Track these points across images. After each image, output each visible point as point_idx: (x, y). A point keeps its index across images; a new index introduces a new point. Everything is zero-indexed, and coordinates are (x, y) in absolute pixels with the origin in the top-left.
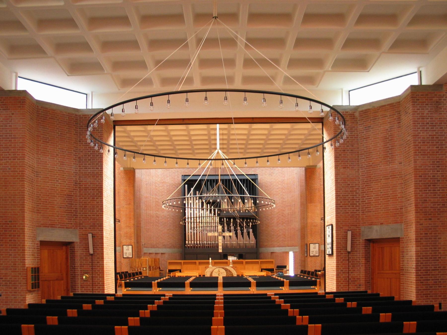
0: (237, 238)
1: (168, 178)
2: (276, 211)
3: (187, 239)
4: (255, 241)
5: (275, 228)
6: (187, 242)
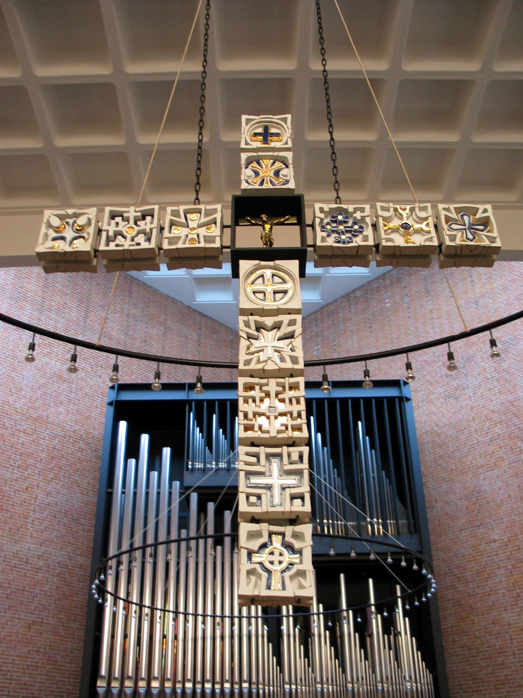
0: (343, 665)
1: (61, 409)
2: (497, 538)
3: (103, 671)
4: (430, 677)
5: (506, 616)
6: (101, 684)
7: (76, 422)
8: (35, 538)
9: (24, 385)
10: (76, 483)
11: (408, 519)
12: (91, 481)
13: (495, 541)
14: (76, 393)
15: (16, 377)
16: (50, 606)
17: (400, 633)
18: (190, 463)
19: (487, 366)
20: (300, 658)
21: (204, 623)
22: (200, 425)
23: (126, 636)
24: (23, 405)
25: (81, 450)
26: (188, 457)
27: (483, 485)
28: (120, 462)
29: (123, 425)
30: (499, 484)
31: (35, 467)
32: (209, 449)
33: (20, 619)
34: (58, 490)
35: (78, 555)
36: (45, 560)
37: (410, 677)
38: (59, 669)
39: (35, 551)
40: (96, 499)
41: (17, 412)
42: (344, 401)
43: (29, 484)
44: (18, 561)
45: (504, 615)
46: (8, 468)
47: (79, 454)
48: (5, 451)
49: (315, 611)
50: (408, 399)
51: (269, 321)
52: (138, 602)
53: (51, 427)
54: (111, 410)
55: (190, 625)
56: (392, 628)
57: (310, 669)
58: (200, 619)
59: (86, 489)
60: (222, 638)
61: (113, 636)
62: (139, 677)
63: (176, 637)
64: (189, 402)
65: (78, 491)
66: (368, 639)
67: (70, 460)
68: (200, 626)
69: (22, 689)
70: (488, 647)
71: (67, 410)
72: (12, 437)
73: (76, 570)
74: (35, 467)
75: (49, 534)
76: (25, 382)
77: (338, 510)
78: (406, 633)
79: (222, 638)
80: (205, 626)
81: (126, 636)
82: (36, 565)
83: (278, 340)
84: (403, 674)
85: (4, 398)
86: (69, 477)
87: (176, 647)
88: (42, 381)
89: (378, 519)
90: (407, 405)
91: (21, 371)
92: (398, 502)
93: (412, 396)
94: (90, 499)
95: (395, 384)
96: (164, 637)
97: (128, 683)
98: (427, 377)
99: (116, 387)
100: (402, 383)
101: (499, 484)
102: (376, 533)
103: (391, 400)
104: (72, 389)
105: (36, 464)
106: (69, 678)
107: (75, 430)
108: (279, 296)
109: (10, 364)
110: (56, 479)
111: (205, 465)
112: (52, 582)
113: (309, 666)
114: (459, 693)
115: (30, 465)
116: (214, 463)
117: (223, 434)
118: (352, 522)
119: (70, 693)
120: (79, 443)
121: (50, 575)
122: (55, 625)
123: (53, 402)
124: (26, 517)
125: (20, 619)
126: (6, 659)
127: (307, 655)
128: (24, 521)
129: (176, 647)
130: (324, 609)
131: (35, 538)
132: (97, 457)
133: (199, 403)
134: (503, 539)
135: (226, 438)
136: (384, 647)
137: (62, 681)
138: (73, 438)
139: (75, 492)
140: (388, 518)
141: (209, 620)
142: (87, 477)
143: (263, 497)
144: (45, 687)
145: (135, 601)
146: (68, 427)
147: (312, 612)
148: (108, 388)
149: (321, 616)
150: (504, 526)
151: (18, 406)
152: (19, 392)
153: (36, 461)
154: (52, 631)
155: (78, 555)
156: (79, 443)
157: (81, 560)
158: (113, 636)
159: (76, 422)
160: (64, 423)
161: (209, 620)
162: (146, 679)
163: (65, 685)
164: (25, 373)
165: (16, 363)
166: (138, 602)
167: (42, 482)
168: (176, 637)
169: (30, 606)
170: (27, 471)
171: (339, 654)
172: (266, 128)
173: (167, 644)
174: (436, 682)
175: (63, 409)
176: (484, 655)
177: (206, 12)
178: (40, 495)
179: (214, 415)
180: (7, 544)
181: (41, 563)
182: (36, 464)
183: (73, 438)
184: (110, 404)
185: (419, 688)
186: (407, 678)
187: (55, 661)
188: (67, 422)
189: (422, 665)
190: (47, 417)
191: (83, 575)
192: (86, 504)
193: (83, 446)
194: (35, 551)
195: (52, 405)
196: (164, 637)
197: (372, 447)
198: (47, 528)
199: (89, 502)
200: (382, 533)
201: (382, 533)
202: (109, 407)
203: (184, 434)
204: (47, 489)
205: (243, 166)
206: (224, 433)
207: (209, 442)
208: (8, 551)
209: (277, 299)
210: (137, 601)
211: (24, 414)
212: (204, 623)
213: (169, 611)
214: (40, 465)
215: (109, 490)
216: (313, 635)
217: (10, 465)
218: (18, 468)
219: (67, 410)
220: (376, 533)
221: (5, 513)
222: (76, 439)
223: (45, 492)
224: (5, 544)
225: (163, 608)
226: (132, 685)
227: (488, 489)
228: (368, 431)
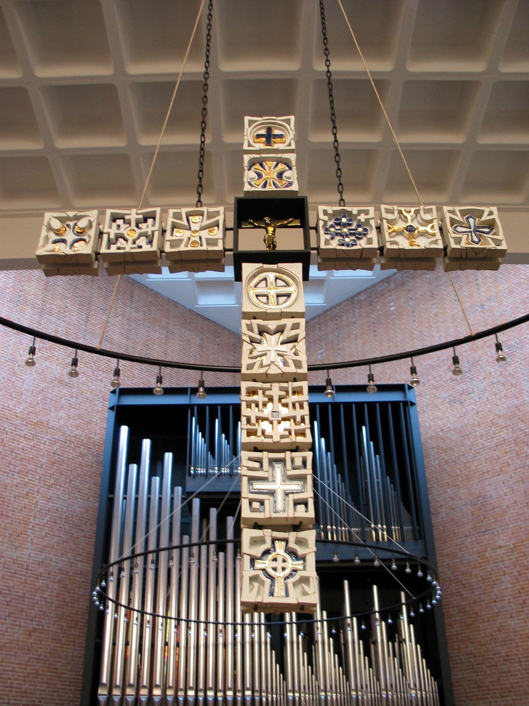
1: (62, 414)
2: (502, 544)
3: (105, 679)
4: (435, 685)
5: (512, 623)
6: (102, 692)
7: (77, 427)
8: (36, 544)
9: (25, 389)
10: (77, 489)
11: (413, 525)
12: (92, 486)
13: (500, 547)
14: (77, 398)
15: (16, 381)
16: (51, 613)
17: (404, 640)
18: (192, 468)
19: (492, 370)
20: (304, 665)
21: (206, 630)
22: (202, 430)
23: (127, 643)
24: (23, 409)
25: (82, 455)
26: (190, 463)
27: (489, 491)
28: (121, 467)
29: (124, 430)
30: (505, 490)
31: (35, 472)
32: (211, 454)
33: (20, 626)
34: (59, 495)
35: (79, 561)
36: (45, 566)
37: (415, 685)
38: (60, 677)
39: (36, 557)
40: (97, 505)
41: (17, 416)
42: (348, 406)
43: (30, 490)
44: (19, 567)
45: (510, 622)
46: (8, 473)
47: (80, 459)
48: (6, 456)
49: (319, 618)
50: (413, 404)
51: (272, 325)
52: (140, 609)
53: (51, 431)
54: (113, 414)
55: (192, 632)
56: (397, 635)
57: (314, 677)
58: (202, 626)
59: (87, 494)
60: (225, 645)
61: (114, 643)
62: (141, 685)
63: (178, 645)
64: (191, 406)
65: (79, 497)
66: (372, 646)
67: (71, 465)
68: (202, 633)
69: (22, 696)
70: (493, 655)
71: (67, 414)
72: (12, 442)
73: (76, 577)
74: (35, 472)
75: (50, 541)
76: (26, 386)
77: (342, 516)
78: (410, 641)
79: (225, 645)
80: (207, 633)
81: (127, 643)
82: (36, 571)
83: (281, 344)
84: (408, 682)
85: (4, 402)
86: (70, 483)
87: (178, 655)
88: (43, 385)
89: (382, 525)
90: (412, 410)
91: (21, 375)
92: (403, 508)
93: (417, 400)
94: (91, 505)
95: (400, 388)
96: (166, 644)
97: (129, 691)
98: (432, 382)
99: (117, 391)
100: (406, 387)
101: (505, 490)
102: (381, 539)
103: (395, 405)
104: (73, 393)
105: (36, 469)
106: (70, 686)
107: (76, 435)
108: (282, 299)
109: (10, 368)
110: (57, 485)
111: (207, 471)
112: (53, 589)
113: (312, 673)
114: (464, 701)
115: (31, 470)
116: (216, 468)
117: (226, 439)
118: (356, 528)
119: (71, 701)
120: (80, 448)
121: (51, 581)
122: (56, 632)
123: (54, 406)
124: (26, 523)
125: (20, 626)
126: (6, 666)
127: (310, 663)
128: (24, 527)
129: (178, 655)
130: (328, 616)
131: (36, 544)
132: (98, 463)
133: (201, 408)
134: (509, 545)
135: (228, 443)
136: (389, 655)
137: (63, 689)
138: (74, 443)
139: (76, 498)
140: (393, 524)
141: (211, 627)
142: (88, 483)
143: (266, 503)
144: (46, 695)
145: (136, 608)
146: (69, 432)
147: (315, 619)
148: (109, 393)
149: (325, 623)
150: (509, 532)
151: (18, 410)
152: (20, 396)
153: (37, 466)
154: (53, 639)
155: (79, 561)
156: (80, 448)
157: (82, 567)
158: (114, 643)
159: (77, 427)
160: (64, 428)
161: (211, 627)
162: (148, 687)
163: (66, 693)
164: (25, 377)
165: (16, 367)
166: (140, 609)
167: (43, 487)
168: (178, 645)
169: (30, 613)
170: (27, 476)
171: (343, 662)
172: (269, 130)
173: (169, 651)
174: (441, 690)
175: (64, 413)
176: (490, 662)
177: (208, 12)
178: (41, 501)
179: (217, 420)
180: (7, 550)
181: (41, 569)
182: (36, 469)
183: (74, 443)
184: (112, 408)
185: (424, 696)
186: (412, 686)
187: (56, 669)
188: (68, 426)
189: (427, 673)
190: (48, 422)
191: (84, 582)
192: (87, 510)
193: (84, 452)
194: (36, 557)
195: (52, 409)
196: (166, 644)
197: (377, 452)
198: (48, 534)
199: (90, 507)
200: (386, 539)
201: (386, 539)
202: (111, 411)
203: (187, 439)
204: (47, 494)
205: (246, 168)
206: (227, 438)
207: (211, 447)
208: (8, 558)
209: (280, 302)
210: (139, 607)
211: (24, 419)
212: (206, 630)
213: (171, 618)
214: (40, 470)
215: (110, 496)
216: (317, 642)
217: (10, 470)
218: (19, 473)
219: (67, 414)
220: (381, 539)
221: (5, 519)
222: (77, 444)
223: (45, 497)
224: (5, 550)
225: (165, 615)
226: (134, 693)
227: (494, 494)
228: (373, 436)
